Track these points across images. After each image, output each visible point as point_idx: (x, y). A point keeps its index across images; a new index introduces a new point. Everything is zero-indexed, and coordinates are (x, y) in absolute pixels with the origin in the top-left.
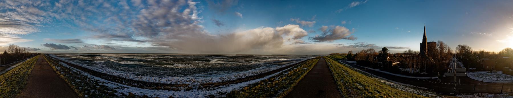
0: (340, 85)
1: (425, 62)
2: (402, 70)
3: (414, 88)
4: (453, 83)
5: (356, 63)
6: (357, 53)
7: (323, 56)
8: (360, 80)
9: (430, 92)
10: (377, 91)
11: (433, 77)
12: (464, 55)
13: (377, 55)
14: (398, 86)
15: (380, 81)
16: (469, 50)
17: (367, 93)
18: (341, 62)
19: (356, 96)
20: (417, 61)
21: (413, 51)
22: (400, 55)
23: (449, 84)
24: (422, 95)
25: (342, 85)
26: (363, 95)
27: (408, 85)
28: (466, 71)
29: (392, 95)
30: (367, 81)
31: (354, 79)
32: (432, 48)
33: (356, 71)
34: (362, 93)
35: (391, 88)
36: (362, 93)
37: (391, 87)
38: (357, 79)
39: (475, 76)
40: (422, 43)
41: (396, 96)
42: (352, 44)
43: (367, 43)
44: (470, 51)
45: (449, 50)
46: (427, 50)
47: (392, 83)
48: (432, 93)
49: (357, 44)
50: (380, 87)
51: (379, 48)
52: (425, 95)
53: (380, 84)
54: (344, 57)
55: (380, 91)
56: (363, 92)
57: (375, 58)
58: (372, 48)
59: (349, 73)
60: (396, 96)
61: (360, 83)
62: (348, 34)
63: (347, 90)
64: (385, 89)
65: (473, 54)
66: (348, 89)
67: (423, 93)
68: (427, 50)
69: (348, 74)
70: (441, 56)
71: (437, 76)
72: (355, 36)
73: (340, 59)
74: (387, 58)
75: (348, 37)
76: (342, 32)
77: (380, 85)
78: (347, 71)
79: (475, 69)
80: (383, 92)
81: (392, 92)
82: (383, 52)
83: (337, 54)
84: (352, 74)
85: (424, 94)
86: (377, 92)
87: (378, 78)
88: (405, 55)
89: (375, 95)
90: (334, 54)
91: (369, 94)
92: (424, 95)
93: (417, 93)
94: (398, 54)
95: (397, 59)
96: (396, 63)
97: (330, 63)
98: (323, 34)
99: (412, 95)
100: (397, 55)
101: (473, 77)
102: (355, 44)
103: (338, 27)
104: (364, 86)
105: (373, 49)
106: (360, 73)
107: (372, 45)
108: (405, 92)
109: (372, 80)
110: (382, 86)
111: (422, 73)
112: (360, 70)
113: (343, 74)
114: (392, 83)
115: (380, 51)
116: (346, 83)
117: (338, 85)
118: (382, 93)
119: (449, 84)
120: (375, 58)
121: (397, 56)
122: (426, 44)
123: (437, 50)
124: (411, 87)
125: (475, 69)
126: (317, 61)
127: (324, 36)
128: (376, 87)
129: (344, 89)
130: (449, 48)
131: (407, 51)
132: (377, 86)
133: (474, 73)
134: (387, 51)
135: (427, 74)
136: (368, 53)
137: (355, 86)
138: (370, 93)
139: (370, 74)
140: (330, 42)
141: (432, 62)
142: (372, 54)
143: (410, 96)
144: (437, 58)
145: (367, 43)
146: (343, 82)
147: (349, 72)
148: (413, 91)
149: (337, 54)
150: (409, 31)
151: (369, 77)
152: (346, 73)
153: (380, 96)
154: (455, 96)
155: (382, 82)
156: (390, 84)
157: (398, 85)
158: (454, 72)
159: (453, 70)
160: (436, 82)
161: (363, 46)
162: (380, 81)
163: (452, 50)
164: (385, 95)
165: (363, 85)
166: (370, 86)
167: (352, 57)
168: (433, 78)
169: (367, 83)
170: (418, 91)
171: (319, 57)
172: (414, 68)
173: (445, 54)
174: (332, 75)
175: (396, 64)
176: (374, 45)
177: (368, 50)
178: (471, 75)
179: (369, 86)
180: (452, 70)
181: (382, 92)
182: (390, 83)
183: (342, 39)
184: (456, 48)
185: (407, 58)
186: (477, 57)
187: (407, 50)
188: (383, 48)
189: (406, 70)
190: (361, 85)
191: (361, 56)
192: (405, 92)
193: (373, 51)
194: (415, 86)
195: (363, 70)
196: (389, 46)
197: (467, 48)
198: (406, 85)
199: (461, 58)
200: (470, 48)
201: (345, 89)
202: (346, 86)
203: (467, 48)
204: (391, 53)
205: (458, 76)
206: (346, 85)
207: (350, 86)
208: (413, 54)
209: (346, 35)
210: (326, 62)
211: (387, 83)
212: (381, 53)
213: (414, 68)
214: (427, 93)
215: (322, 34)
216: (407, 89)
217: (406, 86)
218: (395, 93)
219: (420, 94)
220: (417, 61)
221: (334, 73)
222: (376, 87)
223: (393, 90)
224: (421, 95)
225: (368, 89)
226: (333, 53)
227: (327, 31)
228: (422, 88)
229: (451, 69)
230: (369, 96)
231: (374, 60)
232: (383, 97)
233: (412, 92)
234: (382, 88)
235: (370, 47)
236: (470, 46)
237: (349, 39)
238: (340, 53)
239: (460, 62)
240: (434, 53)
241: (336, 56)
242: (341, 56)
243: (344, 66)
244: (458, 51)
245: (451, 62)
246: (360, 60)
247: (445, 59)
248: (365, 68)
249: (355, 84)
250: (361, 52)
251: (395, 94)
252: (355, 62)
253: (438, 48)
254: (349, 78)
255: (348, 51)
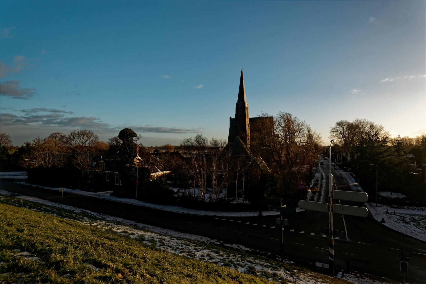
2: (177, 193)
3: (210, 247)
4: (325, 233)
5: (27, 177)
6: (32, 142)
9: (257, 261)
11: (266, 210)
12: (358, 149)
13: (104, 150)
14: (165, 243)
16: (376, 135)
20: (219, 167)
22: (172, 151)
23: (313, 234)
24: (235, 267)
27: (193, 237)
28: (370, 201)
29: (146, 270)
37: (145, 246)
39: (405, 222)
40: (233, 117)
41: (159, 272)
43: (71, 113)
44: (380, 139)
45: (310, 136)
46: (249, 138)
47: (148, 231)
48: (263, 262)
49: (34, 114)
51: (112, 130)
52: (243, 269)
53: (109, 239)
57: (96, 159)
58: (88, 129)
60: (159, 272)
65: (390, 147)
67: (238, 261)
68: (249, 138)
70: (288, 154)
71: (278, 208)
74: (135, 159)
77: (108, 242)
79: (401, 196)
81: (145, 261)
82: (122, 142)
85: (241, 266)
87: (104, 219)
92: (240, 269)
94: (167, 147)
95: (165, 160)
96: (160, 173)
99: (207, 267)
100: (164, 151)
101: (397, 224)
102: (23, 111)
105: (90, 134)
108: (184, 258)
109: (83, 228)
111: (232, 201)
112: (42, 202)
114: (149, 234)
115: (112, 140)
118: (109, 266)
119: (313, 234)
121: (165, 154)
122: (248, 122)
123: (276, 138)
124: (204, 242)
125: (404, 196)
130: (309, 131)
133: (398, 211)
134: (134, 138)
135: (247, 202)
136: (73, 142)
139: (78, 211)
143: (200, 272)
144: (277, 158)
145: (71, 113)
148: (208, 255)
150: (200, 86)
151: (72, 221)
153: (100, 278)
154: (332, 276)
155: (115, 232)
158: (326, 200)
159: (323, 193)
160: (274, 227)
161: (59, 121)
162: (110, 230)
163: (319, 138)
164: (118, 271)
165: (42, 250)
166: (70, 248)
168: (264, 214)
173: (299, 147)
175: (161, 177)
176: (97, 121)
177: (73, 135)
178: (385, 217)
179: (64, 252)
180: (320, 195)
181: (110, 263)
182: (142, 233)
184: (330, 130)
185: (193, 160)
186: (411, 156)
187: (192, 137)
188: (122, 129)
189: (190, 193)
192: (184, 258)
193: (91, 139)
194: (215, 241)
195: (50, 200)
196: (143, 125)
197: (367, 129)
198: (188, 236)
199: (349, 159)
200: (381, 128)
203: (367, 129)
204: (146, 145)
205: (341, 215)
208: (210, 148)
211: (133, 234)
213: (212, 188)
214: (250, 262)
216: (191, 248)
217: (190, 240)
218: (156, 262)
219: (229, 266)
223: (150, 254)
224: (233, 268)
228: (235, 246)
229: (318, 189)
231: (94, 163)
232: (111, 278)
236: (377, 123)
239: (345, 170)
240: (269, 146)
244: (336, 140)
245: (317, 171)
246: (40, 168)
247: (298, 161)
248: (59, 193)
251: (157, 265)
253: (279, 131)
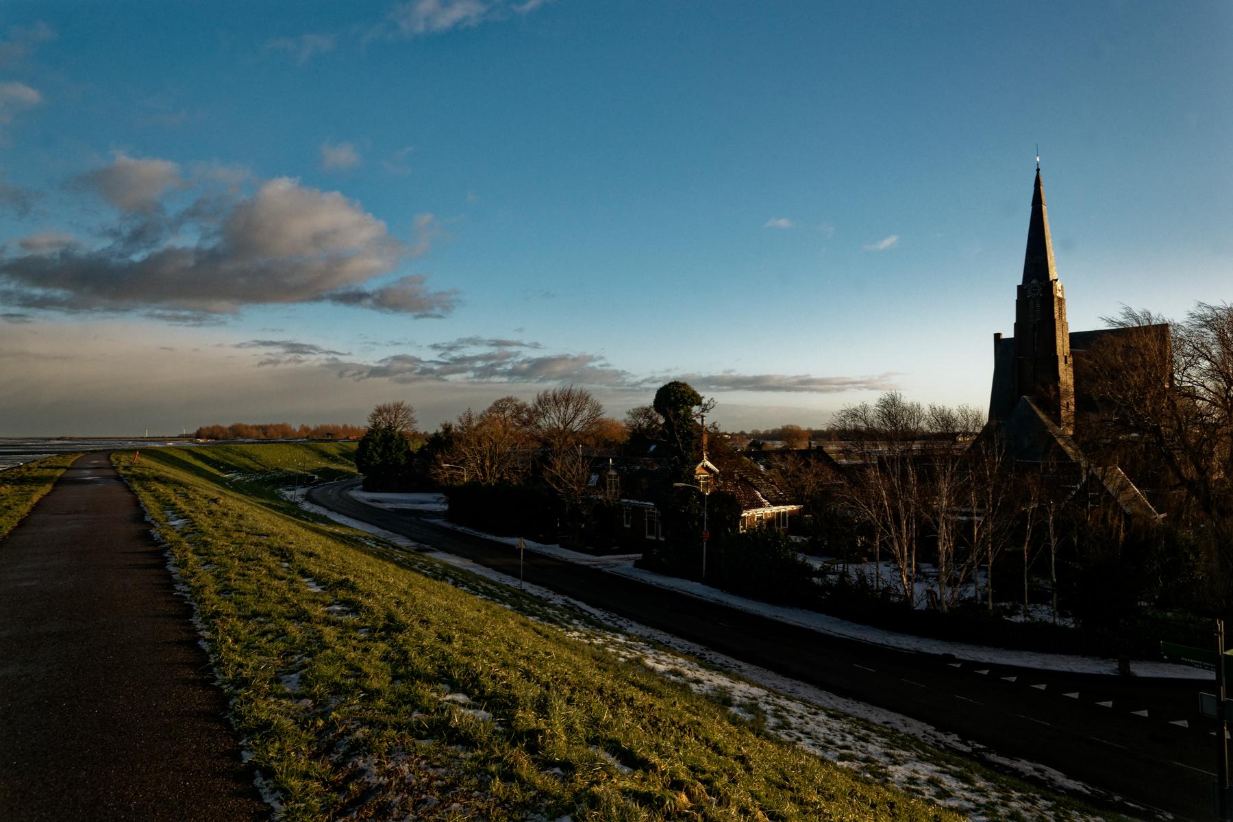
0: (268, 724)
1: (1042, 510)
2: (822, 573)
5: (446, 507)
6: (455, 423)
7: (108, 453)
8: (469, 654)
10: (614, 748)
14: (793, 720)
15: (638, 661)
17: (525, 766)
18: (307, 506)
19: (435, 798)
20: (960, 496)
21: (926, 410)
22: (803, 445)
25: (288, 723)
26: (497, 785)
27: (879, 716)
30: (528, 658)
31: (422, 651)
32: (1136, 379)
33: (442, 574)
34: (481, 771)
35: (733, 729)
36: (481, 771)
37: (734, 721)
38: (446, 648)
40: (1008, 333)
42: (412, 352)
43: (536, 346)
46: (1069, 405)
47: (739, 678)
49: (455, 354)
50: (638, 713)
51: (635, 388)
53: (642, 688)
54: (334, 459)
55: (640, 752)
56: (498, 760)
57: (597, 465)
58: (577, 387)
59: (369, 602)
61: (470, 685)
62: (375, 263)
63: (337, 767)
64: (682, 729)
66: (347, 756)
68: (1069, 405)
69: (355, 608)
72: (434, 285)
73: (291, 480)
74: (698, 468)
75: (370, 286)
76: (318, 239)
77: (641, 698)
78: (353, 588)
80: (663, 755)
82: (662, 421)
83: (269, 435)
84: (398, 603)
86: (611, 760)
87: (619, 630)
88: (848, 445)
89: (595, 789)
90: (237, 432)
91: (542, 780)
93: (978, 808)
94: (788, 434)
95: (783, 473)
96: (769, 511)
97: (180, 514)
98: (126, 232)
100: (779, 445)
102: (435, 347)
103: (280, 189)
104: (502, 705)
105: (584, 398)
106: (475, 590)
107: (580, 360)
109: (574, 647)
110: (659, 704)
111: (1012, 613)
112: (478, 570)
113: (309, 620)
116: (334, 702)
117: (250, 732)
118: (654, 767)
120: (597, 465)
121: (782, 453)
122: (1063, 346)
124: (914, 738)
126: (24, 509)
127: (137, 257)
128: (607, 716)
129: (303, 765)
131: (871, 414)
132: (615, 702)
135: (1069, 623)
136: (543, 422)
137: (426, 711)
138: (554, 764)
139: (558, 600)
140: (199, 321)
141: (1128, 517)
142: (580, 437)
146: (299, 697)
147: (368, 596)
148: (931, 782)
149: (264, 429)
150: (888, 242)
151: (545, 627)
152: (345, 602)
155: (652, 671)
156: (723, 689)
157: (792, 706)
161: (509, 367)
162: (638, 661)
164: (677, 785)
165: (495, 695)
166: (558, 704)
167: (409, 453)
168: (1141, 670)
169: (527, 675)
170: (981, 791)
171: (60, 461)
172: (936, 564)
174: (192, 642)
175: (771, 522)
176: (596, 364)
179: (542, 707)
181: (655, 759)
183: (318, 298)
185: (872, 473)
187: (871, 400)
188: (660, 385)
189: (862, 578)
190: (480, 699)
191: (486, 446)
193: (586, 413)
194: (952, 739)
195: (497, 569)
196: (717, 370)
198: (860, 710)
201: (315, 756)
202: (331, 726)
206: (324, 715)
207: (371, 724)
208: (926, 437)
209: (357, 265)
210: (140, 513)
211: (698, 681)
212: (644, 422)
213: (936, 564)
215: (115, 234)
216: (875, 749)
217: (867, 724)
218: (778, 778)
220: (966, 503)
221: (216, 614)
222: (607, 716)
223: (752, 746)
225: (533, 734)
226: (227, 424)
227: (173, 209)
228: (1025, 766)
230: (544, 794)
231: (594, 478)
232: (662, 801)
233: (929, 792)
234: (654, 723)
235: (561, 377)
237: (385, 301)
238: (296, 427)
241: (258, 450)
242: (300, 453)
243: (333, 536)
246: (473, 485)
248: (513, 551)
249: (428, 693)
250: (486, 420)
252: (433, 503)
254: (366, 650)
255: (372, 410)
